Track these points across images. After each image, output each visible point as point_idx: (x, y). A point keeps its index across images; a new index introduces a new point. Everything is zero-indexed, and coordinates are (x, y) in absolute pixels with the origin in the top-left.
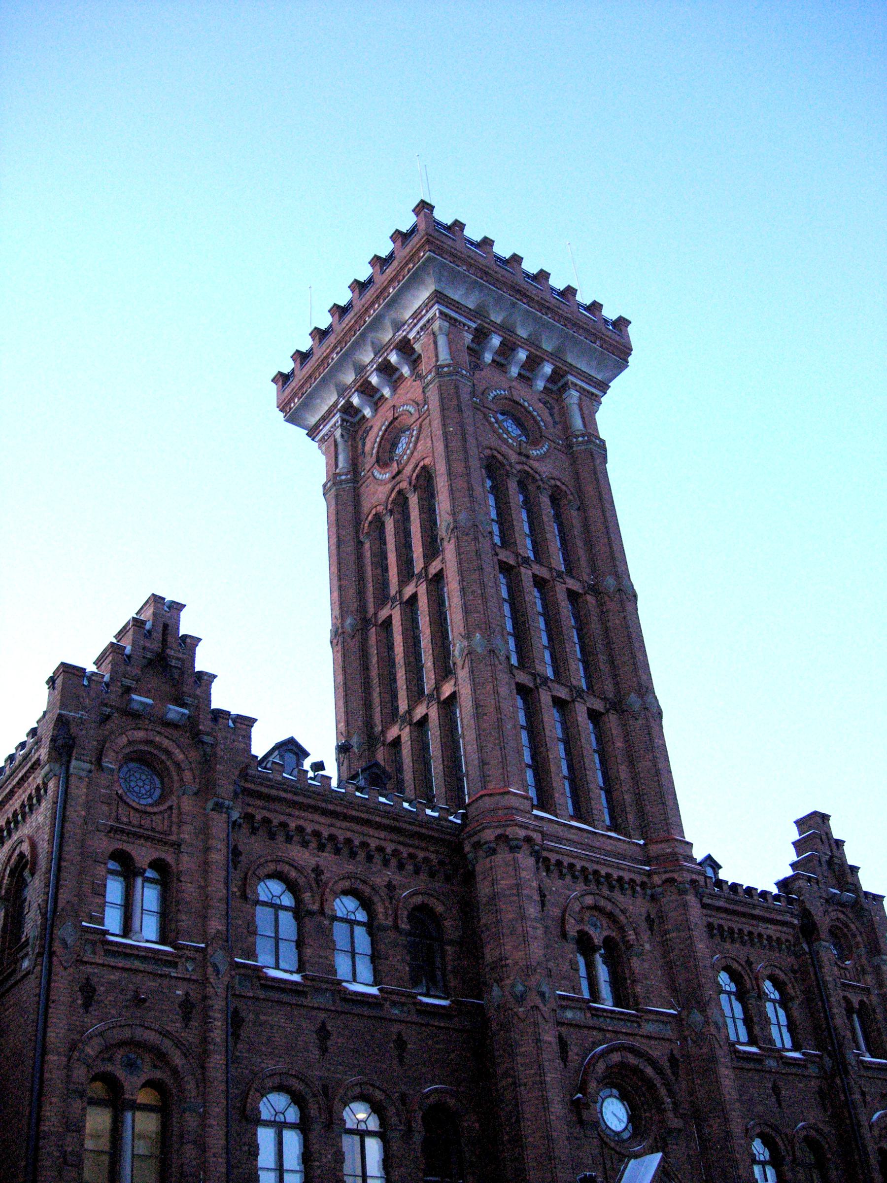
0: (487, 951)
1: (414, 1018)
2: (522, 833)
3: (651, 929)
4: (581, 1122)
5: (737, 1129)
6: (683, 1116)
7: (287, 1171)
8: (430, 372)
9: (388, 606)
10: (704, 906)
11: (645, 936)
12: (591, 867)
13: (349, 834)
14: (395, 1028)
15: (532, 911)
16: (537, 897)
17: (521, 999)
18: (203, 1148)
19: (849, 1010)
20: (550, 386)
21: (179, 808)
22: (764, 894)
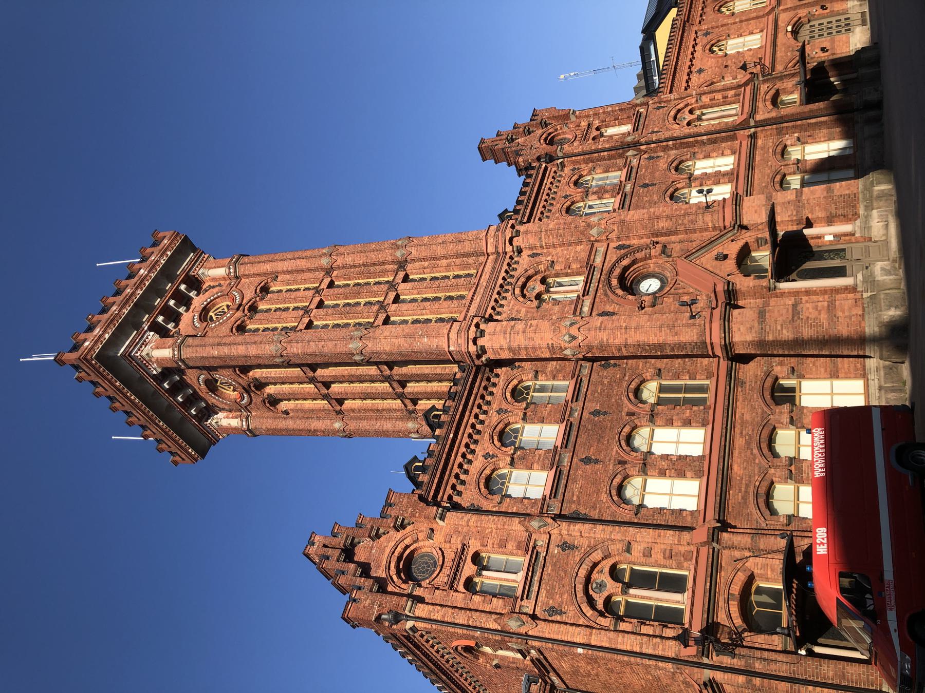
1: (581, 403)
2: (473, 328)
7: (808, 503)
10: (529, 221)
11: (542, 258)
12: (497, 289)
14: (586, 415)
17: (574, 338)
22: (525, 184)
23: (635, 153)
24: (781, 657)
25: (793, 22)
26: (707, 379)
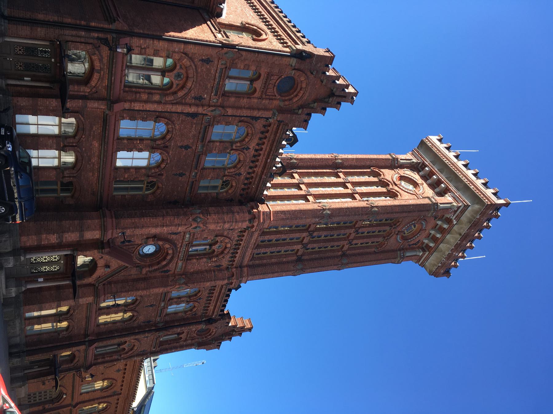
0: (213, 208)
1: (191, 180)
3: (217, 266)
4: (148, 238)
5: (140, 293)
6: (146, 274)
8: (436, 200)
9: (352, 188)
12: (241, 247)
13: (260, 161)
14: (188, 174)
15: (227, 226)
16: (231, 228)
17: (194, 220)
18: (146, 102)
19: (179, 334)
20: (425, 245)
21: (275, 99)
22: (224, 306)
23: (158, 325)
24: (69, 38)
25: (63, 399)
26: (114, 196)
